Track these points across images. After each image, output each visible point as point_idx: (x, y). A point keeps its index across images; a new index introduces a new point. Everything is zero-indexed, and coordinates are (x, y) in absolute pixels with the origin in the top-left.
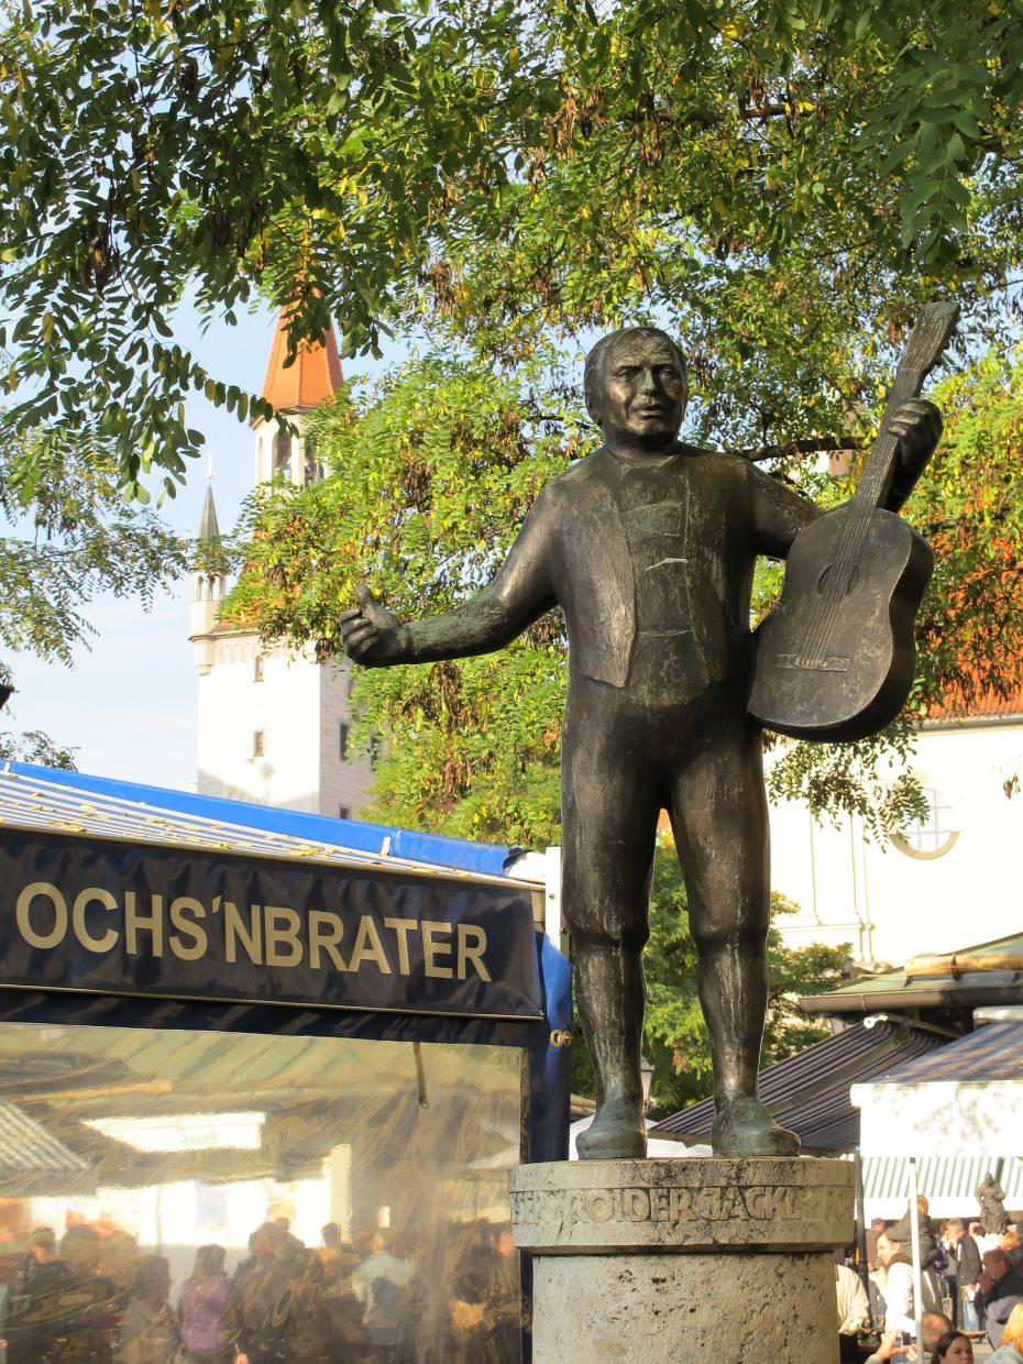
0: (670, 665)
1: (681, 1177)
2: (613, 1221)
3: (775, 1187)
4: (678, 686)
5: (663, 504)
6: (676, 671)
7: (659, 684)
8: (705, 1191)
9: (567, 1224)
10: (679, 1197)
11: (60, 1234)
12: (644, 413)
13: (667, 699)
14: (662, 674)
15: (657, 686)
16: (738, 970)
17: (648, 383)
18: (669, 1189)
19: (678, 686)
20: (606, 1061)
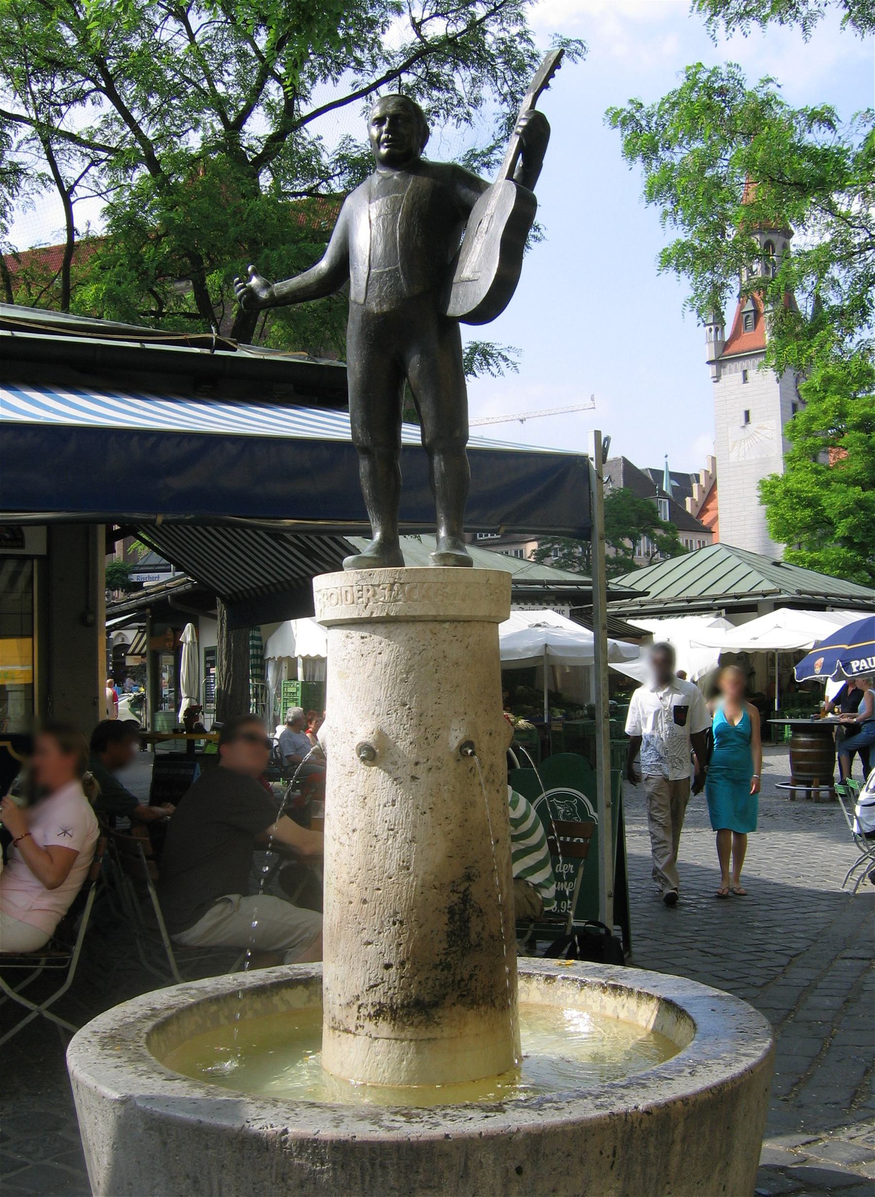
10: (368, 590)
13: (385, 308)
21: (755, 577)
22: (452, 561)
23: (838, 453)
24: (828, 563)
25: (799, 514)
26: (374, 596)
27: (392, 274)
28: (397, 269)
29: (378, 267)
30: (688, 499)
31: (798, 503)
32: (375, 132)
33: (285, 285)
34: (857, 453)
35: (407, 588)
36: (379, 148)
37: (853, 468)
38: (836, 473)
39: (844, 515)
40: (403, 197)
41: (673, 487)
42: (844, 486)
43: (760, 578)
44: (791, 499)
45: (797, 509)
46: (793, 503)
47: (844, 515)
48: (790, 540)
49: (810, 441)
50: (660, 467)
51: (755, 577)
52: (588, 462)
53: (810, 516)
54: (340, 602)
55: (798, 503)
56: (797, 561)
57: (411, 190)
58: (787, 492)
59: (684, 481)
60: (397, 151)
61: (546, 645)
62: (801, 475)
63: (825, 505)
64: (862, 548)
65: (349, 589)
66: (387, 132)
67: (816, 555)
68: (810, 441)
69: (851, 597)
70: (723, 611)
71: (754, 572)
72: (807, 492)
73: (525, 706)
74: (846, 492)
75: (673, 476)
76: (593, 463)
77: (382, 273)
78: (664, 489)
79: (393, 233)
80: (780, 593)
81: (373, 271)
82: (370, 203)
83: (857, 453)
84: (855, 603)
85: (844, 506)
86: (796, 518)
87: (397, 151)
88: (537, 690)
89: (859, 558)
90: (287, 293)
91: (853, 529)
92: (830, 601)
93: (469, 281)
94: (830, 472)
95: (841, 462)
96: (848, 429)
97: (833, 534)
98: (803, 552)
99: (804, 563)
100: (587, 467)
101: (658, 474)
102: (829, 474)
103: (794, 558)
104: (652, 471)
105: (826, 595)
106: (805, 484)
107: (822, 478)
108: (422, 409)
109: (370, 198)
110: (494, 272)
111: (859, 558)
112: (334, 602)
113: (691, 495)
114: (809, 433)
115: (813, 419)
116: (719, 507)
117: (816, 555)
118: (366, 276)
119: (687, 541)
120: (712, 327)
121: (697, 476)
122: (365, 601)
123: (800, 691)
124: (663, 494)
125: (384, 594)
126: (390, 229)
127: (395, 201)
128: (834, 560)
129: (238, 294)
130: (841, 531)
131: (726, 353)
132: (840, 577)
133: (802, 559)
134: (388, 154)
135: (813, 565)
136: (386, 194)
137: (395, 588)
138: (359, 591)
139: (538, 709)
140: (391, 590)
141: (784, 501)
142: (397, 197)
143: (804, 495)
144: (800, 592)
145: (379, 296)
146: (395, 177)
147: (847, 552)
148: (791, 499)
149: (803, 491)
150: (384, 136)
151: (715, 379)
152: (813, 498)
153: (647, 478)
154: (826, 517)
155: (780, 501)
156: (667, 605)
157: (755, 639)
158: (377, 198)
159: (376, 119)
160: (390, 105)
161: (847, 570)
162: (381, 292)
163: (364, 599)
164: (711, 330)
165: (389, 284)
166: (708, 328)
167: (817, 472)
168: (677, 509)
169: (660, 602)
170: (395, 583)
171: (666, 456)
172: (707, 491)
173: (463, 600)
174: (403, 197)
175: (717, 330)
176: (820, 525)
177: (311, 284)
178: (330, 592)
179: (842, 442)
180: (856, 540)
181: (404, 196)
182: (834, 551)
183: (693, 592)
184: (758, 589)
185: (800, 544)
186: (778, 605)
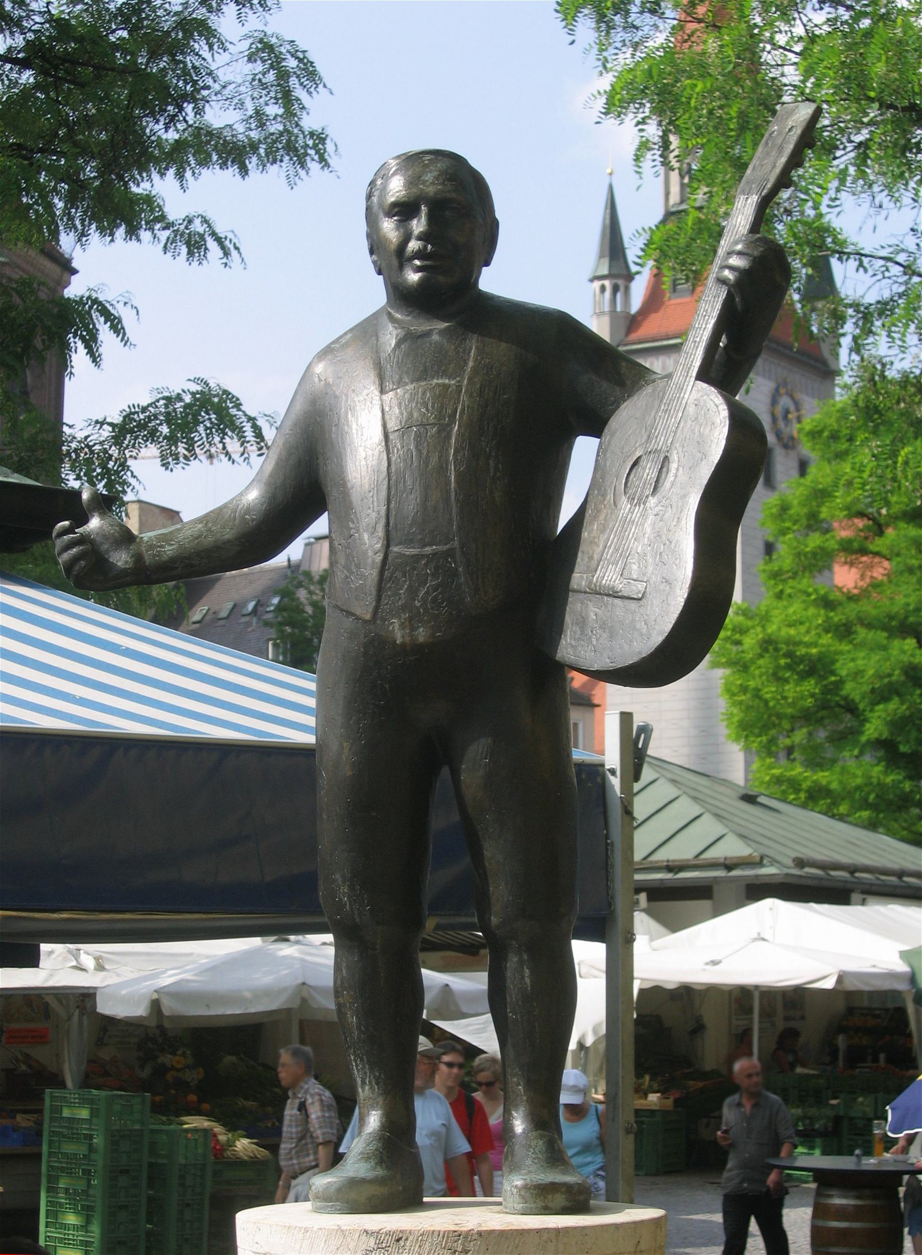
0: (427, 593)
6: (435, 600)
12: (417, 262)
13: (422, 634)
15: (411, 619)
16: (527, 972)
17: (418, 225)
20: (363, 1083)
21: (708, 828)
23: (870, 567)
24: (848, 794)
25: (791, 690)
28: (450, 553)
29: (408, 541)
31: (789, 667)
34: (911, 570)
36: (401, 267)
37: (900, 600)
38: (868, 608)
39: (881, 695)
40: (459, 388)
42: (882, 636)
43: (720, 829)
44: (776, 659)
45: (786, 681)
46: (778, 667)
47: (881, 695)
48: (772, 741)
49: (814, 541)
51: (708, 828)
52: (604, 778)
53: (813, 695)
55: (789, 667)
56: (787, 788)
57: (475, 371)
58: (768, 645)
60: (441, 279)
61: (304, 984)
62: (795, 608)
63: (844, 673)
64: (917, 765)
67: (822, 777)
68: (814, 541)
69: (901, 874)
70: (643, 897)
71: (707, 818)
72: (808, 645)
73: (241, 1102)
74: (885, 648)
76: (615, 782)
77: (417, 558)
79: (442, 468)
80: (760, 864)
82: (382, 391)
83: (911, 570)
84: (909, 886)
85: (881, 678)
86: (785, 698)
87: (441, 279)
88: (265, 1066)
89: (907, 786)
90: (173, 560)
91: (898, 725)
92: (860, 882)
93: (615, 594)
94: (852, 605)
95: (876, 585)
96: (894, 519)
97: (855, 732)
98: (797, 770)
99: (797, 791)
100: (602, 787)
102: (851, 611)
103: (778, 780)
105: (853, 869)
106: (803, 629)
107: (837, 617)
108: (487, 854)
111: (907, 786)
114: (814, 523)
115: (822, 495)
117: (822, 777)
118: (379, 558)
120: (607, 283)
123: (799, 1070)
126: (434, 460)
128: (858, 788)
129: (66, 556)
130: (874, 728)
131: (633, 336)
132: (872, 826)
133: (794, 785)
134: (422, 283)
135: (815, 797)
136: (422, 375)
139: (270, 1109)
141: (761, 662)
143: (801, 651)
144: (800, 863)
146: (435, 337)
147: (886, 773)
148: (776, 659)
149: (800, 643)
150: (413, 245)
152: (821, 657)
154: (845, 698)
155: (753, 661)
157: (715, 963)
159: (395, 205)
161: (886, 811)
164: (603, 289)
166: (597, 284)
167: (827, 603)
174: (459, 388)
175: (615, 289)
176: (834, 713)
177: (229, 541)
179: (879, 544)
180: (903, 748)
181: (462, 383)
182: (860, 769)
184: (716, 853)
185: (790, 750)
186: (757, 891)
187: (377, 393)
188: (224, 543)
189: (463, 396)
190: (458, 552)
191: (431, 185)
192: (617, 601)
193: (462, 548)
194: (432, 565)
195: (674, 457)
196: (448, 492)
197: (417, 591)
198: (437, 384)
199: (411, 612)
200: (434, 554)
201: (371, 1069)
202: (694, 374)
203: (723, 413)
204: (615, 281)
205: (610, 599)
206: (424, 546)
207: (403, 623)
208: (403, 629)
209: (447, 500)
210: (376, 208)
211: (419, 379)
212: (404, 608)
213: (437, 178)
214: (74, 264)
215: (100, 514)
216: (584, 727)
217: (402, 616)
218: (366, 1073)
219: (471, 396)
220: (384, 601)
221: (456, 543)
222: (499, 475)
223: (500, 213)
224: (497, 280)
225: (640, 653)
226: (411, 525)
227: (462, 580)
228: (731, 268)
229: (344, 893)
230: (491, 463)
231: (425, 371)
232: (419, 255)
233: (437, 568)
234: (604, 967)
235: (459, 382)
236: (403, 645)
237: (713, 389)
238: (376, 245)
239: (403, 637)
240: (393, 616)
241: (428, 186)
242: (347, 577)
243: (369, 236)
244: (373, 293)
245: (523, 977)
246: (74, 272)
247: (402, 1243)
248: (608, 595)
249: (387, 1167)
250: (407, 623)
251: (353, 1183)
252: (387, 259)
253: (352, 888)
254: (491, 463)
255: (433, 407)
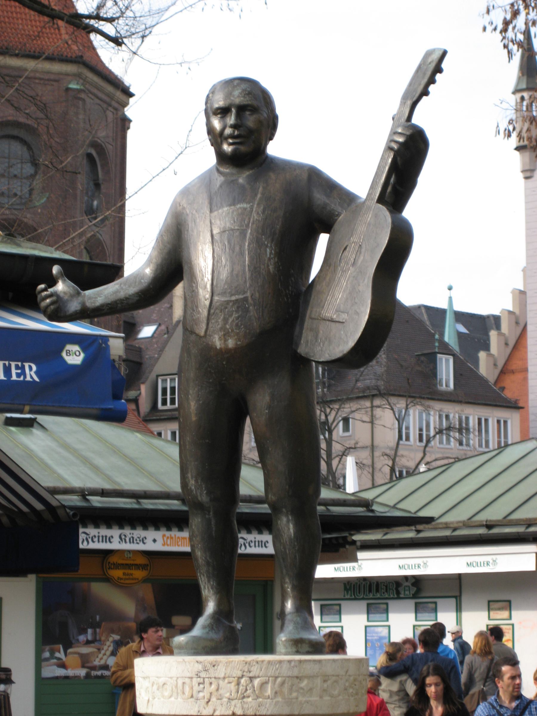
0: (233, 321)
1: (212, 670)
2: (173, 699)
3: (276, 678)
4: (237, 334)
5: (239, 206)
6: (237, 325)
7: (226, 335)
8: (226, 681)
9: (151, 699)
10: (211, 683)
11: (196, 463)
12: (231, 141)
13: (231, 343)
14: (228, 327)
15: (224, 335)
16: (291, 526)
17: (231, 119)
18: (204, 678)
19: (237, 334)
20: (205, 588)
22: (306, 648)
26: (217, 690)
27: (241, 305)
28: (245, 299)
29: (223, 293)
30: (482, 355)
32: (217, 124)
33: (99, 294)
35: (256, 682)
41: (460, 335)
50: (441, 303)
54: (175, 694)
57: (261, 199)
59: (479, 327)
65: (187, 681)
66: (234, 127)
75: (460, 317)
77: (228, 302)
78: (446, 339)
81: (216, 298)
82: (211, 211)
87: (242, 148)
90: (102, 306)
93: (332, 321)
101: (437, 315)
104: (428, 308)
109: (211, 204)
110: (365, 318)
112: (167, 694)
113: (486, 347)
116: (530, 369)
119: (480, 420)
120: (526, 95)
121: (497, 319)
122: (207, 696)
124: (446, 349)
125: (228, 689)
127: (243, 215)
134: (234, 152)
137: (243, 681)
138: (199, 684)
140: (238, 684)
142: (245, 209)
145: (223, 329)
151: (528, 174)
153: (420, 322)
156: (457, 533)
158: (222, 206)
159: (218, 109)
160: (237, 93)
162: (225, 324)
163: (206, 694)
164: (523, 98)
165: (235, 315)
166: (519, 95)
168: (465, 372)
169: (446, 526)
170: (243, 676)
171: (450, 288)
172: (512, 343)
173: (321, 697)
178: (161, 681)
183: (496, 513)
187: (208, 212)
188: (130, 296)
189: (254, 214)
190: (250, 299)
191: (237, 98)
192: (333, 324)
193: (251, 296)
194: (236, 306)
195: (364, 246)
196: (245, 266)
197: (228, 319)
198: (241, 208)
199: (224, 331)
200: (237, 300)
201: (209, 581)
202: (376, 201)
203: (389, 220)
204: (531, 93)
205: (330, 323)
206: (232, 295)
207: (220, 337)
208: (221, 340)
209: (244, 271)
210: (209, 110)
211: (233, 204)
212: (221, 329)
213: (241, 93)
214: (132, 90)
215: (62, 280)
216: (512, 422)
217: (220, 333)
218: (206, 583)
219: (258, 213)
220: (210, 325)
221: (248, 294)
222: (272, 256)
223: (278, 111)
224: (275, 149)
225: (343, 351)
226: (225, 284)
227: (252, 313)
228: (396, 142)
229: (192, 485)
230: (268, 250)
231: (234, 200)
232: (232, 136)
233: (238, 307)
234: (179, 462)
235: (252, 206)
236: (221, 349)
237: (384, 207)
238: (210, 131)
239: (220, 345)
240: (215, 334)
241: (236, 98)
242: (191, 313)
243: (207, 125)
244: (210, 158)
245: (289, 529)
246: (131, 95)
247: (216, 667)
248: (329, 320)
249: (215, 632)
250: (222, 337)
251: (196, 639)
252: (216, 138)
253: (196, 481)
254: (268, 250)
255: (237, 220)
